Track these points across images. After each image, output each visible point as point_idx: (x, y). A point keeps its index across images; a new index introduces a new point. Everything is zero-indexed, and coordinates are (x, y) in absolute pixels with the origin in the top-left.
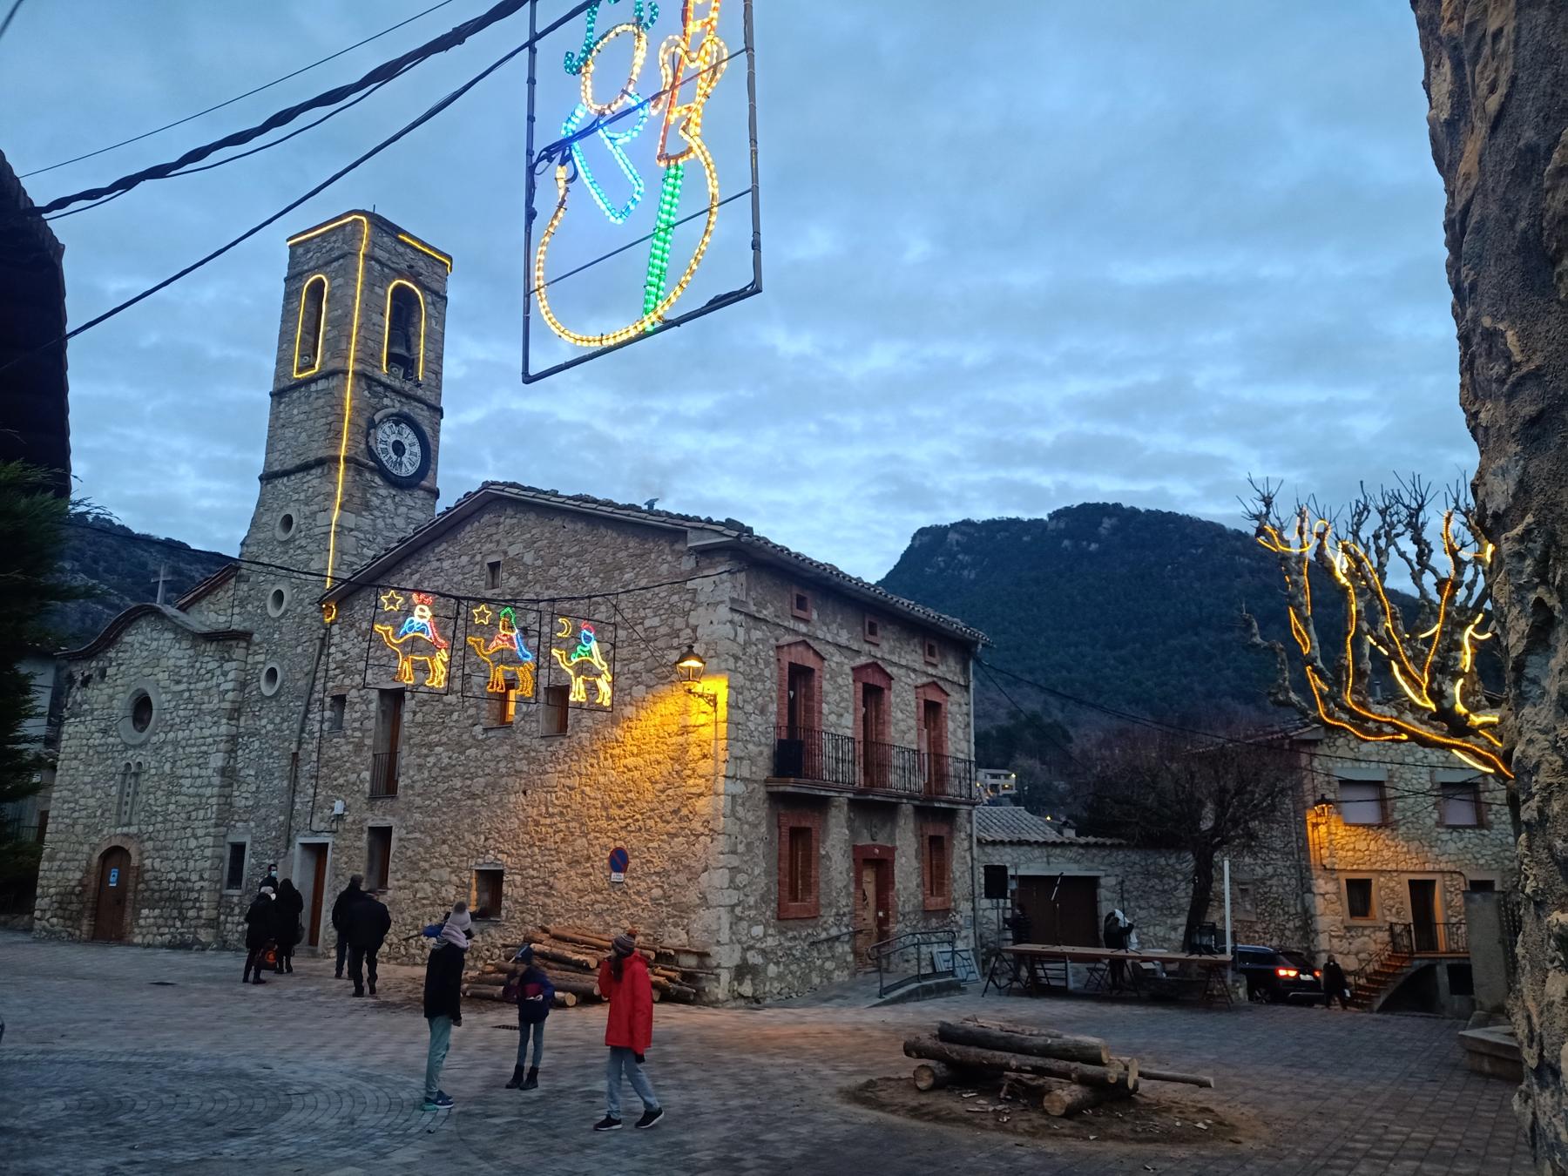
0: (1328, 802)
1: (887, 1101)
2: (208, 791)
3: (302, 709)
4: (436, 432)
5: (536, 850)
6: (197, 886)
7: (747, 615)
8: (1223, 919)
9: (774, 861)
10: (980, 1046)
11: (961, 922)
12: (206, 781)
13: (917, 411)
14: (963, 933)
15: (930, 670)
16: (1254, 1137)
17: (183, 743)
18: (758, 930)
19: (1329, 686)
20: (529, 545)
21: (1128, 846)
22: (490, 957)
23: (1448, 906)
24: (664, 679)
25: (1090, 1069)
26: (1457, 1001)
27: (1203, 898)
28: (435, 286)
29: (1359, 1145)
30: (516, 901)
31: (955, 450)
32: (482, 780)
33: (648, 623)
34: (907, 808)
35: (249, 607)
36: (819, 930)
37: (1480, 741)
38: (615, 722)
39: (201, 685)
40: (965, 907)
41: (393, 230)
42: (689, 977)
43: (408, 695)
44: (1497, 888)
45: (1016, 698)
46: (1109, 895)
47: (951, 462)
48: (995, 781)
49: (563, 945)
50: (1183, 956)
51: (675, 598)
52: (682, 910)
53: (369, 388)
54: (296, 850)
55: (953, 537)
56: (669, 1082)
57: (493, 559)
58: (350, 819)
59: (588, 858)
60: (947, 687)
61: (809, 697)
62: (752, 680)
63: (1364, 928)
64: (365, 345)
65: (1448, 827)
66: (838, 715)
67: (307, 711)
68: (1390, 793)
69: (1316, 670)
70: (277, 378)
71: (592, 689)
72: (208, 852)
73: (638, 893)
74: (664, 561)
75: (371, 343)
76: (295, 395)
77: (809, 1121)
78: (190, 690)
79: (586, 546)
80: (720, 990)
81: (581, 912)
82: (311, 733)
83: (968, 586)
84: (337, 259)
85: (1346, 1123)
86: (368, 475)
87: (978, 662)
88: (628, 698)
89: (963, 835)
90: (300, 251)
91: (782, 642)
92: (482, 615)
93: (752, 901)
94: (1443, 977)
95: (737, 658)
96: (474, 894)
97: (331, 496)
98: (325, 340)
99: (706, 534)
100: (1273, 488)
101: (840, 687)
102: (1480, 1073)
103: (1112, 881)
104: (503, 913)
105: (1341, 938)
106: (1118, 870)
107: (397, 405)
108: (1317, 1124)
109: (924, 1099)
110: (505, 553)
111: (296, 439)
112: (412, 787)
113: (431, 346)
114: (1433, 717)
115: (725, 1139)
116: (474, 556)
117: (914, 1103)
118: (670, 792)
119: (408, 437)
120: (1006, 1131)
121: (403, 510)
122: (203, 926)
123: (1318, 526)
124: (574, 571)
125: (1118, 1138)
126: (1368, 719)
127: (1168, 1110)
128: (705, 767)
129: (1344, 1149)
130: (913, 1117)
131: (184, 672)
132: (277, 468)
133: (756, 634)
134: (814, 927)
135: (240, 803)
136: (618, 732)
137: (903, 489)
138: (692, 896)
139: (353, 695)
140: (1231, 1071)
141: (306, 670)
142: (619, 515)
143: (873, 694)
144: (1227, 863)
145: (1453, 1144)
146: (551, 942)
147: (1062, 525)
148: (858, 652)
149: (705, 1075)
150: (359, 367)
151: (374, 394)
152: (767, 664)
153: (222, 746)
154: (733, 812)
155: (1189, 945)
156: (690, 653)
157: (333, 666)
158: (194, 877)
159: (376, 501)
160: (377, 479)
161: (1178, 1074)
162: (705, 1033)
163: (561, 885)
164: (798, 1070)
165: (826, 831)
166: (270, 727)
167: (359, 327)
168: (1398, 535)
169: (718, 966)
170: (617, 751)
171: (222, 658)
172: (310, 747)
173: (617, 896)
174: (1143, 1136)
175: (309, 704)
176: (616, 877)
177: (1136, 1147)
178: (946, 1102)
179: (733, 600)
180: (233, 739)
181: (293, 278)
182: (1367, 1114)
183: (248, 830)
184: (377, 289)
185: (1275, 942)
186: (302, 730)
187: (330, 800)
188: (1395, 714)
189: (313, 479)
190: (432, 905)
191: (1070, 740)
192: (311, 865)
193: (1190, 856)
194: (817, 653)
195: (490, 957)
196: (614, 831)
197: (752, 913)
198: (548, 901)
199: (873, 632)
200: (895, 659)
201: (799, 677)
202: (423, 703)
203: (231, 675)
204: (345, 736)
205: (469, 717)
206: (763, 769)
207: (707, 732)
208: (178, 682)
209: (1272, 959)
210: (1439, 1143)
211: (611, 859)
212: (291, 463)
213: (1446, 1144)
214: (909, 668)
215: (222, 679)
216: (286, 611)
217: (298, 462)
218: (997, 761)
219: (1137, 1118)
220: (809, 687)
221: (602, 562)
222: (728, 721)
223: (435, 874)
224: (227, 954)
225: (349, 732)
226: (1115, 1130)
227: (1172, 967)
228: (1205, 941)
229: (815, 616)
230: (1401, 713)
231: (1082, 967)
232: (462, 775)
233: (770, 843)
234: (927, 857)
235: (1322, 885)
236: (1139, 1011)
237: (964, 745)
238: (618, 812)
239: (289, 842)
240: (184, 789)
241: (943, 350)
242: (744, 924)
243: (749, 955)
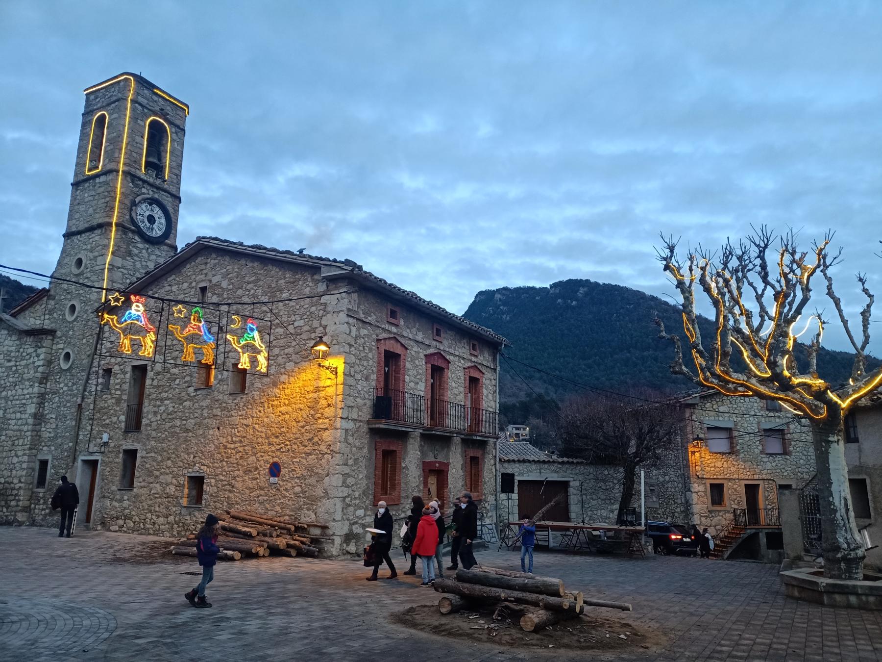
0: (701, 439)
1: (418, 622)
2: (25, 428)
3: (85, 377)
4: (176, 211)
5: (225, 463)
6: (17, 486)
7: (357, 319)
8: (640, 506)
9: (372, 470)
10: (482, 585)
11: (489, 508)
12: (24, 422)
13: (483, 224)
14: (489, 514)
15: (473, 359)
16: (657, 644)
17: (11, 398)
18: (360, 512)
19: (706, 361)
20: (225, 276)
21: (587, 464)
22: (195, 530)
23: (766, 499)
24: (305, 358)
25: (552, 600)
26: (771, 553)
27: (629, 493)
28: (178, 122)
29: (724, 649)
30: (212, 495)
31: (503, 246)
32: (193, 421)
33: (296, 324)
34: (457, 440)
35: (55, 315)
36: (400, 512)
37: (797, 396)
38: (275, 384)
39: (23, 363)
40: (491, 499)
41: (151, 86)
42: (315, 541)
43: (149, 368)
44: (794, 487)
45: (531, 386)
46: (575, 492)
47: (500, 253)
48: (517, 432)
49: (238, 522)
50: (616, 527)
51: (314, 308)
52: (313, 501)
53: (133, 182)
54: (79, 464)
55: (498, 296)
56: (279, 610)
57: (203, 285)
58: (112, 445)
59: (256, 469)
60: (483, 369)
61: (397, 372)
62: (360, 359)
63: (720, 511)
64: (131, 155)
65: (767, 454)
66: (415, 382)
67: (88, 379)
68: (735, 433)
69: (699, 351)
70: (76, 175)
71: (254, 361)
72: (25, 466)
73: (286, 490)
74: (308, 286)
75: (134, 154)
76: (87, 185)
77: (360, 637)
78: (16, 366)
79: (260, 276)
80: (334, 549)
81: (251, 502)
82: (90, 392)
83: (506, 322)
84: (114, 102)
85: (715, 632)
86: (131, 235)
87: (502, 355)
88: (283, 370)
89: (491, 456)
90: (92, 97)
91: (380, 337)
92: (180, 312)
93: (357, 494)
94: (763, 540)
95: (350, 346)
96: (186, 491)
97: (107, 246)
98: (105, 152)
99: (333, 269)
100: (675, 241)
101: (417, 366)
102: (792, 597)
103: (577, 483)
104: (203, 502)
105: (706, 517)
106: (581, 478)
107: (151, 193)
108: (697, 633)
109: (444, 620)
110: (210, 281)
111: (86, 211)
112: (150, 426)
113: (174, 159)
114: (770, 380)
115: (298, 653)
116: (191, 283)
117: (437, 623)
118: (307, 428)
119: (158, 213)
120: (494, 642)
121: (153, 257)
122: (20, 511)
123: (702, 263)
124: (252, 292)
125: (567, 646)
126: (730, 381)
127: (603, 625)
128: (329, 412)
129: (714, 651)
130: (435, 633)
131: (13, 354)
132: (74, 229)
133: (364, 332)
134: (397, 511)
135: (45, 435)
136: (277, 391)
137: (472, 267)
138: (319, 492)
139: (116, 368)
140: (643, 598)
141: (88, 353)
142: (280, 257)
143: (437, 371)
144: (642, 472)
145: (784, 647)
146: (230, 520)
147: (557, 291)
148: (429, 346)
149: (305, 605)
150: (126, 169)
151: (136, 186)
152: (371, 350)
153: (35, 400)
154: (346, 439)
155: (620, 521)
156: (320, 341)
157: (104, 351)
158: (16, 481)
159: (136, 251)
160: (137, 238)
161: (609, 602)
162: (318, 576)
163: (239, 485)
164: (369, 600)
165: (406, 452)
166: (65, 389)
167: (127, 144)
168: (749, 270)
169: (334, 534)
170: (275, 403)
171: (37, 346)
172: (89, 401)
173: (274, 491)
174: (584, 644)
175: (89, 374)
176: (273, 480)
177: (579, 652)
178: (459, 622)
179: (349, 310)
180: (42, 396)
181: (88, 113)
182: (727, 626)
183: (50, 451)
184: (139, 121)
185: (669, 519)
186: (85, 390)
187: (100, 433)
188: (746, 379)
189: (96, 236)
190: (160, 497)
191: (559, 409)
192: (89, 472)
193: (622, 469)
194: (402, 345)
195: (195, 530)
196: (273, 452)
197: (357, 502)
198: (231, 495)
199: (438, 333)
200: (452, 351)
201: (391, 359)
202: (158, 373)
203: (42, 357)
204: (111, 394)
205: (186, 382)
206: (366, 413)
207: (331, 391)
208: (9, 361)
209: (667, 529)
210: (775, 646)
211: (271, 469)
212: (82, 226)
213: (779, 646)
214: (460, 358)
215: (36, 359)
216: (77, 317)
217: (86, 225)
218: (519, 420)
219: (581, 632)
220: (397, 366)
221: (270, 287)
222: (344, 384)
223: (162, 478)
224: (35, 529)
225: (113, 391)
226: (566, 641)
227: (611, 534)
228: (629, 518)
229: (402, 323)
230: (749, 378)
231: (558, 533)
232: (181, 418)
233: (370, 459)
234: (469, 468)
235: (696, 487)
236: (590, 560)
237: (493, 403)
238: (275, 440)
239: (75, 459)
240: (11, 427)
241: (497, 189)
242: (351, 509)
243: (354, 527)
